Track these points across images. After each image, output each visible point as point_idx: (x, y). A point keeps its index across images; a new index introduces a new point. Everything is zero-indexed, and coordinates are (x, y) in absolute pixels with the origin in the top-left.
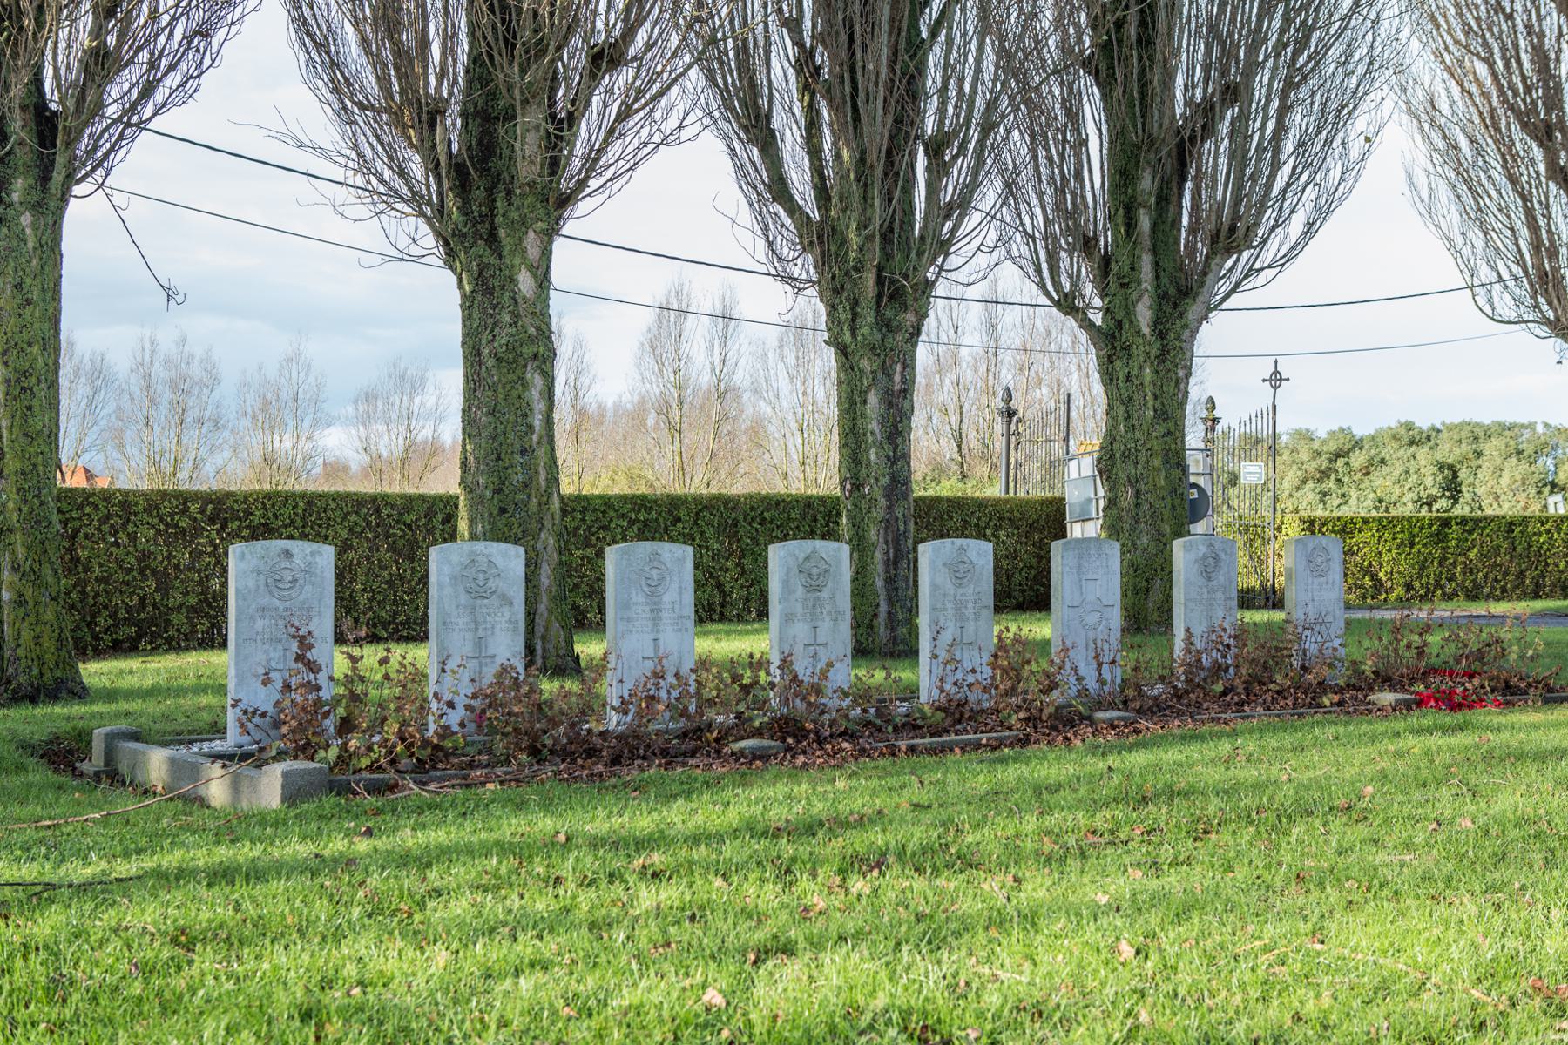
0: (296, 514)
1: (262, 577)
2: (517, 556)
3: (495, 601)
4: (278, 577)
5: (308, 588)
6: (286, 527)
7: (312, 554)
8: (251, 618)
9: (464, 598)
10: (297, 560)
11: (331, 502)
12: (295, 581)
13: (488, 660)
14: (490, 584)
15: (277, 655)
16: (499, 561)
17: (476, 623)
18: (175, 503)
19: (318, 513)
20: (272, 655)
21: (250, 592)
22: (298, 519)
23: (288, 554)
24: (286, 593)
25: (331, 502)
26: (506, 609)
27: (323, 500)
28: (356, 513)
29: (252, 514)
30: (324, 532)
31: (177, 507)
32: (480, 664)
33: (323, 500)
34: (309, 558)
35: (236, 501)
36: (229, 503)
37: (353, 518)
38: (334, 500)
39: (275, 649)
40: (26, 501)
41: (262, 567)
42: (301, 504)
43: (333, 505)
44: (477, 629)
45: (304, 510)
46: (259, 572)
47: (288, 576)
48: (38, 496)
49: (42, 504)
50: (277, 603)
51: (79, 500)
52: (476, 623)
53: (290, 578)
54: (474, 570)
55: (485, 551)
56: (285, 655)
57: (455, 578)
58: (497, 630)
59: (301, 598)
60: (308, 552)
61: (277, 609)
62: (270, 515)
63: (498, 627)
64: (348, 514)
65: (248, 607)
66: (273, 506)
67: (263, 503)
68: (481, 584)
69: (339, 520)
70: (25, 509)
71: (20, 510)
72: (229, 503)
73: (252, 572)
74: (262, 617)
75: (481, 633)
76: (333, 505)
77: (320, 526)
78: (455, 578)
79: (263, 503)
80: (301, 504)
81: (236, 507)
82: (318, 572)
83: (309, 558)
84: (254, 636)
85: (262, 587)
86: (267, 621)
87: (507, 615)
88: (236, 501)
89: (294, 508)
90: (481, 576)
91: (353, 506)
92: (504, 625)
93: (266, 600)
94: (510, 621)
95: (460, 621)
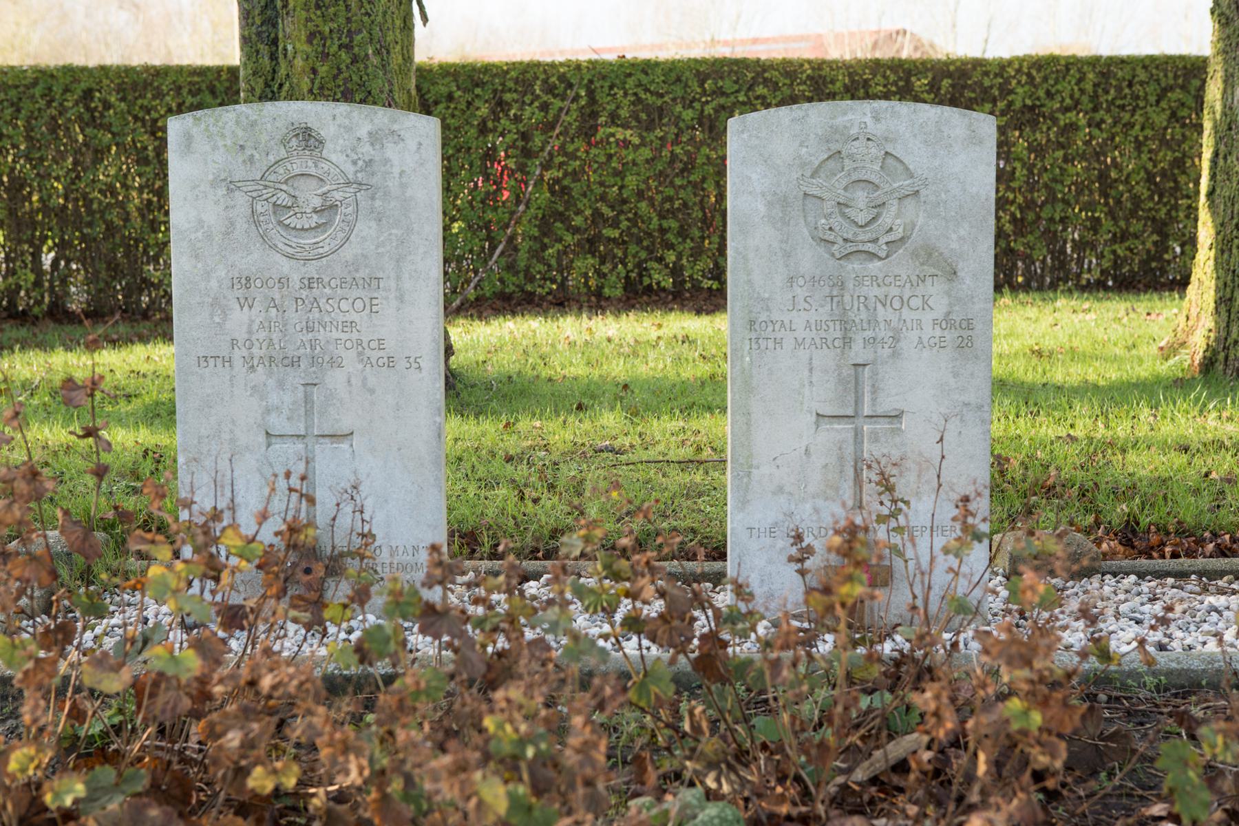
0: (1082, 91)
1: (241, 200)
2: (974, 139)
3: (902, 265)
4: (283, 199)
5: (365, 228)
6: (1067, 110)
7: (375, 138)
8: (215, 303)
9: (808, 258)
10: (335, 154)
11: (1139, 71)
12: (328, 208)
13: (882, 425)
14: (887, 219)
15: (288, 398)
16: (916, 156)
17: (845, 324)
18: (892, 78)
19: (1119, 89)
20: (274, 398)
21: (209, 237)
22: (1085, 99)
23: (307, 137)
24: (308, 240)
25: (1139, 71)
26: (936, 290)
27: (1128, 68)
28: (1183, 87)
29: (1012, 92)
30: (1126, 117)
31: (895, 83)
32: (858, 434)
33: (1128, 68)
34: (366, 149)
35: (986, 74)
36: (976, 76)
37: (1176, 95)
38: (1145, 67)
39: (281, 384)
40: (325, 56)
41: (240, 173)
42: (1091, 76)
43: (1142, 76)
44: (847, 341)
45: (1096, 85)
46: (232, 186)
47: (310, 196)
48: (348, 47)
49: (355, 60)
50: (285, 266)
51: (750, 75)
52: (845, 324)
53: (317, 202)
54: (840, 181)
55: (872, 127)
56: (308, 399)
57: (784, 202)
58: (908, 344)
59: (348, 253)
60: (363, 131)
61: (283, 281)
62: (1041, 93)
63: (913, 335)
64: (1165, 90)
65: (207, 274)
66: (1045, 79)
67: (1029, 75)
68: (862, 218)
69: (1153, 99)
70: (323, 70)
71: (314, 71)
72: (976, 76)
73: (214, 184)
74: (246, 302)
75: (859, 352)
76: (1142, 76)
77: (1122, 107)
78: (784, 202)
79: (1029, 75)
80: (1091, 76)
81: (987, 83)
82: (393, 184)
83: (366, 149)
84: (225, 353)
85: (241, 225)
86: (257, 314)
87: (940, 305)
88: (986, 74)
89: (1078, 83)
90: (861, 197)
91: (1176, 77)
92: (929, 331)
93: (252, 259)
94: (947, 321)
95: (799, 319)
